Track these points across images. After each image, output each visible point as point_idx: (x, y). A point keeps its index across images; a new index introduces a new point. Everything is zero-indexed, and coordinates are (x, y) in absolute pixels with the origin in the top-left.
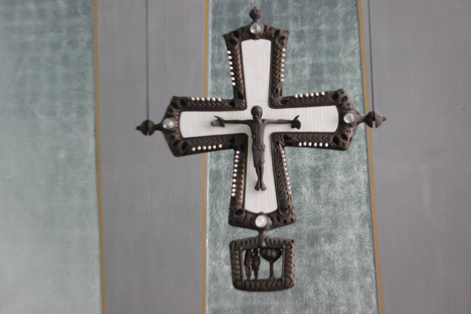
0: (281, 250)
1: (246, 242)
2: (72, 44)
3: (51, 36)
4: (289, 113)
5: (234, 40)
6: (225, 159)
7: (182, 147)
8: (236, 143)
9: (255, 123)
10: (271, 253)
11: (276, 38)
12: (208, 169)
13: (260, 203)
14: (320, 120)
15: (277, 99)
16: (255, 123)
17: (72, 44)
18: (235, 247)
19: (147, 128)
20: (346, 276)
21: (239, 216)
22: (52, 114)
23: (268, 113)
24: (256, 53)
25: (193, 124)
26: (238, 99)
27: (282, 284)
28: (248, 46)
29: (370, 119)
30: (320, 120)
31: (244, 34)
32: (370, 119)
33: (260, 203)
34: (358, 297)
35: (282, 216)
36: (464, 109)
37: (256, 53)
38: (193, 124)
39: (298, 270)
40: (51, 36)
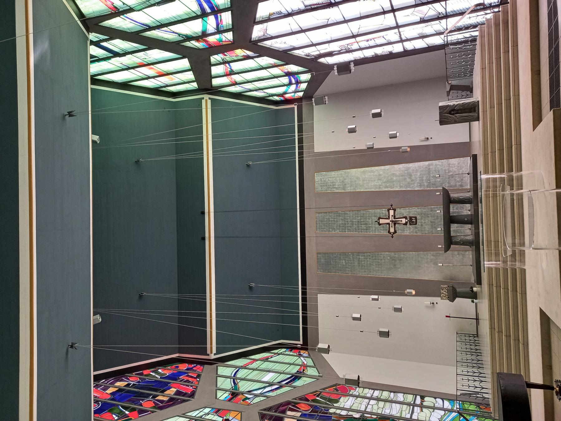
0: (411, 218)
2: (369, 256)
4: (391, 217)
6: (397, 225)
7: (395, 232)
9: (392, 221)
12: (481, 121)
13: (404, 221)
14: (392, 212)
15: (389, 218)
16: (392, 221)
17: (369, 256)
19: (392, 237)
20: (409, 212)
21: (406, 224)
22: (381, 260)
23: (391, 219)
24: (382, 221)
25: (392, 230)
26: (389, 224)
27: (416, 218)
29: (392, 206)
30: (392, 212)
32: (392, 206)
33: (404, 221)
34: (413, 210)
35: (406, 218)
37: (382, 221)
38: (392, 230)
39: (413, 216)
40: (368, 259)
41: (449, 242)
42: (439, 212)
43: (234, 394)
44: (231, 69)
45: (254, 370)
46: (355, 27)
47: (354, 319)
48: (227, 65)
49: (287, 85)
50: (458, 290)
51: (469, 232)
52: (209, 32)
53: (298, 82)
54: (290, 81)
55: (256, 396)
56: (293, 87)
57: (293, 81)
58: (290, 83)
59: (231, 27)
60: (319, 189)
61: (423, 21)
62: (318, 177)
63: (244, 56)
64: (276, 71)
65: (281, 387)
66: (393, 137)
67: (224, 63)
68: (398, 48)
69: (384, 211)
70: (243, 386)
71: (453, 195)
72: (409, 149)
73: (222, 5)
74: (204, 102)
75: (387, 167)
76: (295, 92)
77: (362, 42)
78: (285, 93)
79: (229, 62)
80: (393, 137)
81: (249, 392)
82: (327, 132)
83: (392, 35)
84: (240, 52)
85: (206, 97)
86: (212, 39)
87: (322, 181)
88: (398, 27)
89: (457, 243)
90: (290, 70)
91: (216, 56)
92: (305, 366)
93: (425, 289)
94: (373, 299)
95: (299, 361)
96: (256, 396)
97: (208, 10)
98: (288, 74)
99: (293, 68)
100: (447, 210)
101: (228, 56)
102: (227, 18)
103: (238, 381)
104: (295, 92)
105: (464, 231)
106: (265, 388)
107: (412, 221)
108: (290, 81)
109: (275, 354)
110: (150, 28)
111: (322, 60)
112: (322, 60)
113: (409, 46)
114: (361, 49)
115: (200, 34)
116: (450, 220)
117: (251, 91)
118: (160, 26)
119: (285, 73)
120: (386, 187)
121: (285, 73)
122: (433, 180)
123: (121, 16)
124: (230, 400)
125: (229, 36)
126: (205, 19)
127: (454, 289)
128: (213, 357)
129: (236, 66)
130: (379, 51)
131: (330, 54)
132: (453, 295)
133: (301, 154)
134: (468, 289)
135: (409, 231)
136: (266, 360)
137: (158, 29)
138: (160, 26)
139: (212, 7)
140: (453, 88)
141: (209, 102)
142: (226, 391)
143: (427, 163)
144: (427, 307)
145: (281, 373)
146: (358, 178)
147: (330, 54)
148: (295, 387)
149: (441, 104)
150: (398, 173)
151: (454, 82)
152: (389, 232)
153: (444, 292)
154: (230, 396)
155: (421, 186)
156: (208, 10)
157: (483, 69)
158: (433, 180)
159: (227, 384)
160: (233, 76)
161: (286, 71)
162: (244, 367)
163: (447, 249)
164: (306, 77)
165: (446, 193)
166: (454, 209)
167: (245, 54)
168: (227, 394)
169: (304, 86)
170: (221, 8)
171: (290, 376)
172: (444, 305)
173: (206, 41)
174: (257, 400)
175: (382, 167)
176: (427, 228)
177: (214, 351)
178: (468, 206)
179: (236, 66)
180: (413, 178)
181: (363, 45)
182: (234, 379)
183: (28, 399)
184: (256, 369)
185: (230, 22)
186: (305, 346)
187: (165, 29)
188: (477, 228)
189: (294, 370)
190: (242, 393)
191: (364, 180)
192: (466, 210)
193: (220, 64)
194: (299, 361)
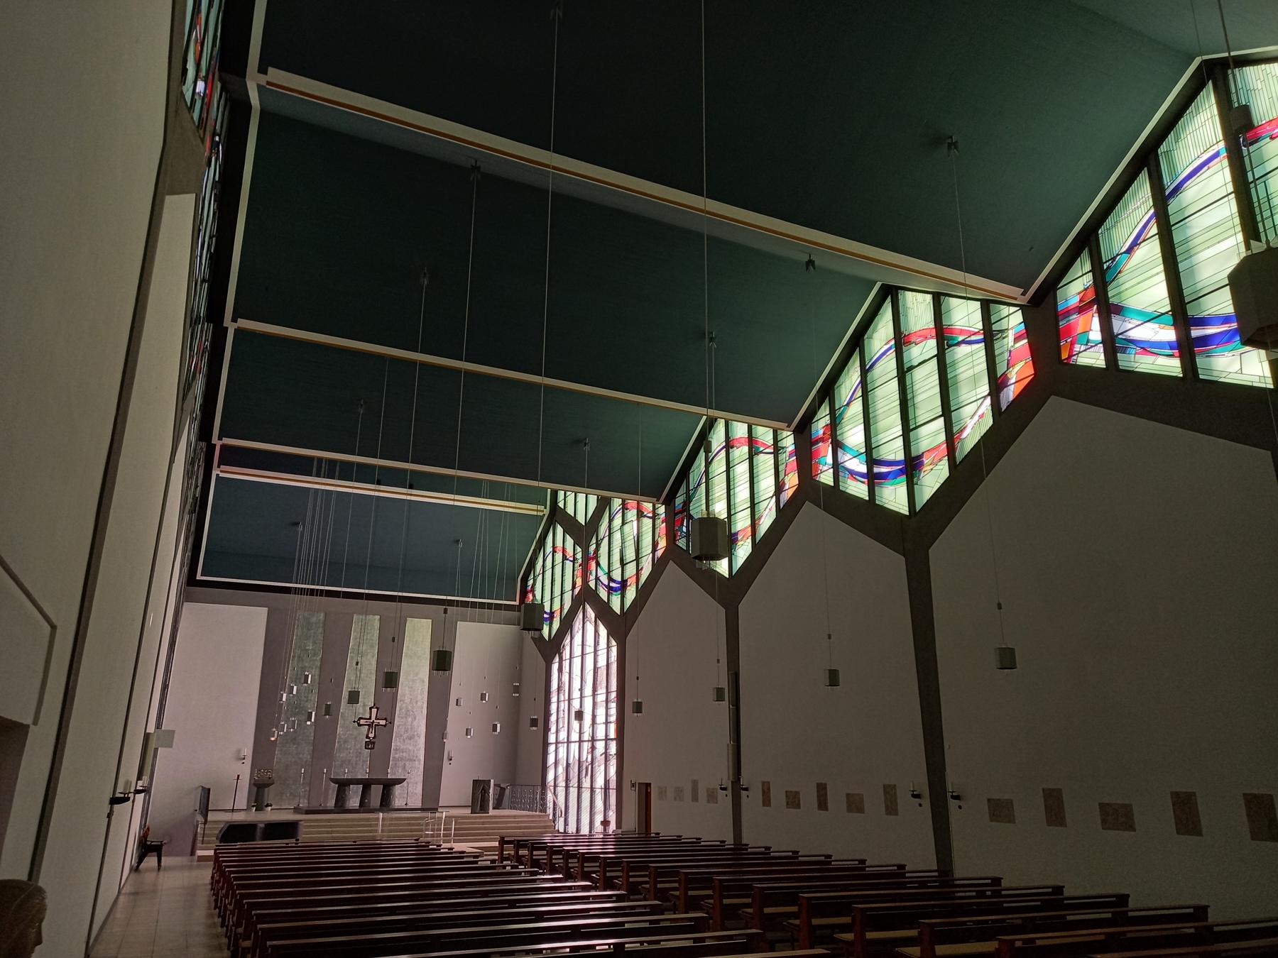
13: (371, 735)
25: (362, 722)
33: (371, 735)
38: (362, 722)
49: (609, 571)
52: (840, 452)
53: (610, 590)
54: (614, 581)
56: (604, 580)
58: (611, 579)
61: (568, 765)
63: (784, 484)
68: (552, 738)
74: (542, 508)
76: (597, 579)
78: (837, 445)
82: (479, 640)
83: (563, 735)
84: (792, 481)
85: (547, 512)
88: (569, 742)
97: (1196, 332)
98: (624, 584)
102: (858, 489)
104: (597, 579)
105: (354, 802)
108: (614, 581)
110: (865, 372)
111: (557, 659)
112: (557, 659)
113: (552, 748)
114: (558, 701)
118: (866, 389)
122: (401, 764)
125: (826, 478)
130: (553, 718)
131: (560, 670)
137: (1156, 214)
138: (866, 389)
140: (503, 790)
143: (422, 758)
144: (239, 751)
147: (560, 670)
150: (415, 723)
151: (507, 792)
157: (515, 817)
161: (926, 461)
164: (616, 607)
166: (376, 791)
169: (603, 594)
172: (245, 770)
173: (822, 440)
179: (765, 462)
181: (562, 704)
183: (45, 652)
186: (190, 580)
187: (859, 393)
192: (354, 802)
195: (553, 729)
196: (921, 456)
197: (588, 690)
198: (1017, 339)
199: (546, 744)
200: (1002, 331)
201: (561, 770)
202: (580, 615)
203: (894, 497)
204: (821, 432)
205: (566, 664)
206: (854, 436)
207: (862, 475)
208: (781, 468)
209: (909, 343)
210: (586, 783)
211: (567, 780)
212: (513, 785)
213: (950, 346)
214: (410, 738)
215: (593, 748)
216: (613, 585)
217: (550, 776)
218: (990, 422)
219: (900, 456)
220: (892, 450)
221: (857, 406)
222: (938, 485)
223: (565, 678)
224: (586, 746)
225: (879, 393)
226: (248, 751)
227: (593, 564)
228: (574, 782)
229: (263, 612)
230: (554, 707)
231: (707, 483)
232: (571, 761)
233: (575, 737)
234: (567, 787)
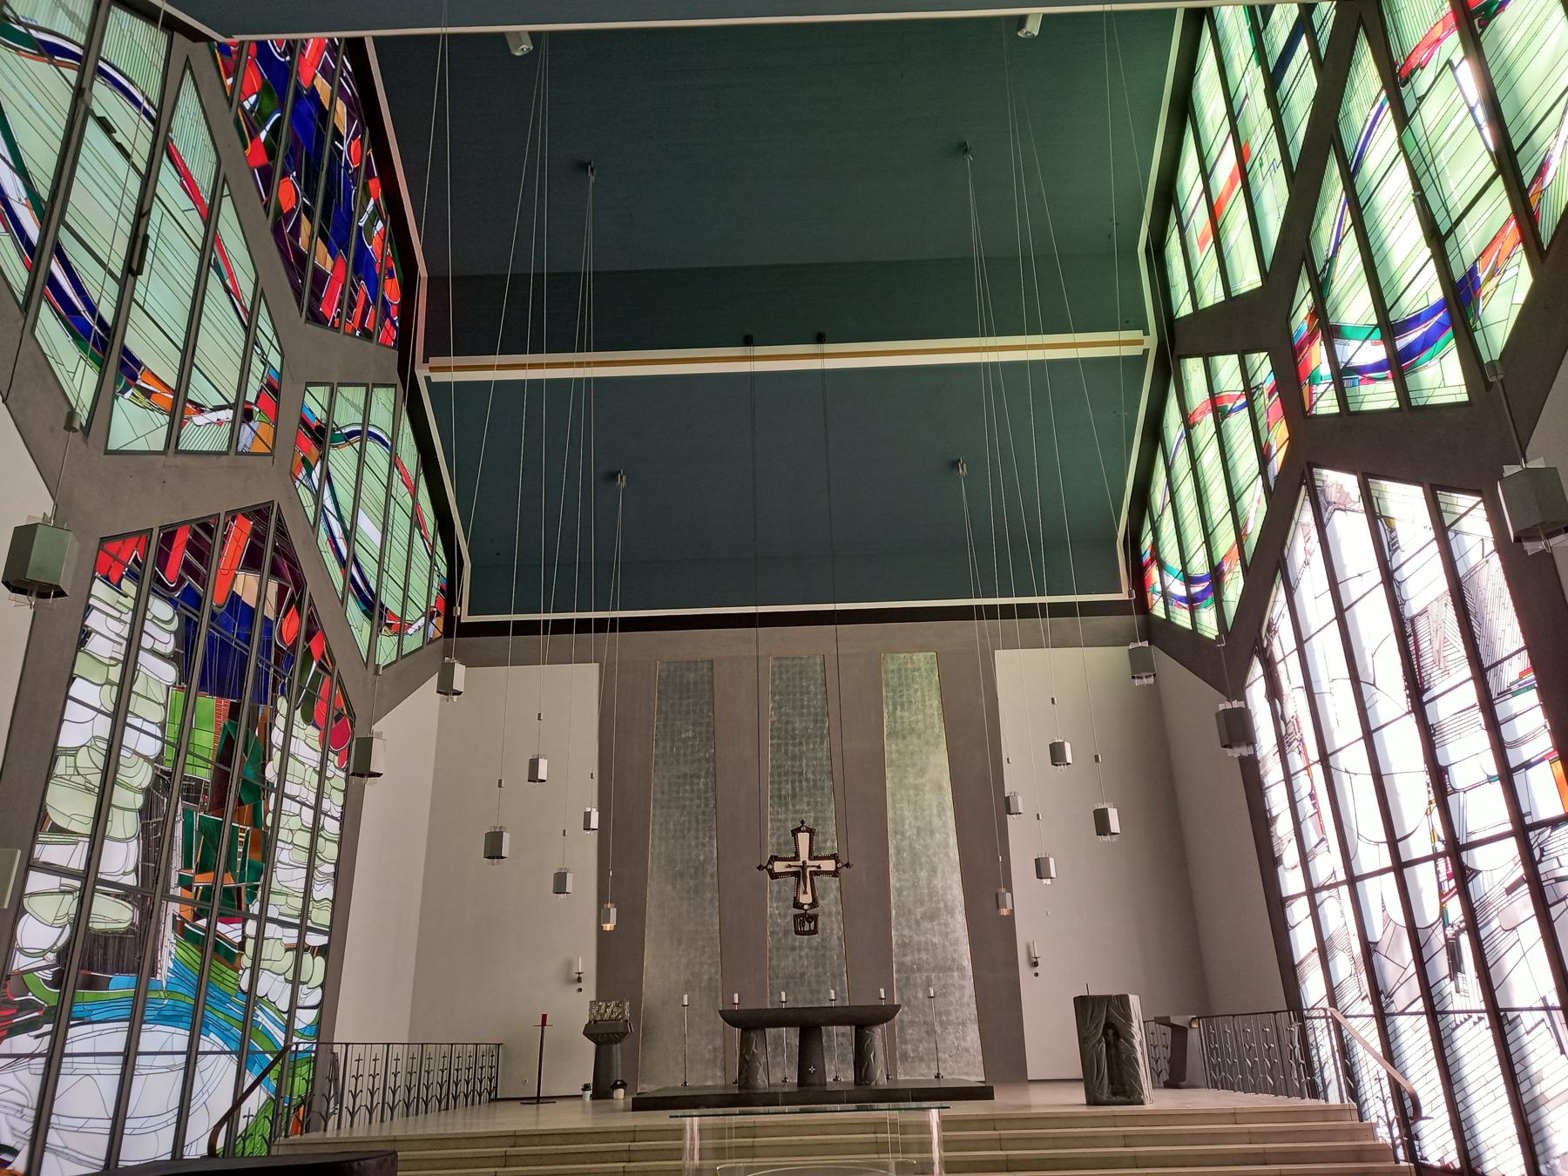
0: (814, 918)
1: (106, 939)
3: (697, 802)
4: (817, 863)
5: (795, 832)
6: (793, 879)
7: (774, 876)
8: (796, 874)
10: (129, 788)
11: (811, 832)
13: (806, 899)
14: (829, 865)
16: (804, 867)
18: (796, 917)
19: (760, 868)
21: (797, 905)
23: (809, 863)
24: (803, 838)
25: (779, 867)
26: (797, 857)
27: (815, 932)
28: (800, 835)
29: (847, 865)
30: (829, 865)
31: (799, 830)
32: (847, 865)
33: (806, 899)
35: (814, 904)
36: (1056, 753)
37: (803, 838)
38: (779, 867)
41: (750, 1024)
42: (832, 997)
43: (321, 435)
44: (1232, 411)
45: (388, 487)
46: (1352, 760)
47: (534, 764)
48: (1243, 400)
50: (617, 1048)
51: (777, 1077)
53: (1192, 602)
54: (1198, 580)
55: (317, 496)
56: (1178, 589)
57: (1196, 589)
59: (1353, 408)
60: (891, 664)
61: (1369, 949)
62: (923, 660)
63: (1269, 447)
64: (1225, 540)
65: (343, 564)
66: (1041, 869)
67: (1250, 391)
68: (1291, 881)
69: (831, 846)
70: (342, 460)
71: (878, 1034)
72: (1004, 912)
73: (1419, 383)
74: (1136, 334)
75: (954, 853)
76: (1165, 594)
77: (1311, 781)
78: (1331, 332)
79: (1250, 404)
80: (1041, 869)
81: (327, 477)
82: (1050, 688)
83: (1327, 864)
84: (1279, 436)
85: (1151, 342)
86: (1317, 356)
87: (914, 672)
88: (1352, 880)
89: (745, 1044)
90: (1228, 578)
91: (1267, 367)
92: (400, 630)
93: (618, 957)
94: (587, 816)
95: (413, 613)
96: (317, 496)
97: (1401, 343)
98: (1216, 575)
99: (1234, 587)
100: (838, 1016)
101: (1266, 403)
102: (1379, 396)
103: (357, 445)
106: (340, 519)
107: (805, 921)
108: (1198, 580)
109: (433, 547)
111: (1257, 669)
112: (1257, 669)
113: (1298, 912)
114: (1288, 778)
115: (1332, 321)
116: (810, 1025)
117: (1169, 469)
118: (1356, 206)
119: (1221, 564)
120: (898, 852)
121: (1221, 564)
122: (919, 978)
123: (1384, 94)
124: (304, 422)
125: (1326, 404)
126: (1377, 334)
127: (619, 1036)
128: (421, 373)
129: (1239, 424)
130: (1283, 828)
131: (1274, 692)
132: (603, 1035)
133: (990, 612)
134: (618, 1075)
135: (778, 913)
136: (416, 521)
138: (1356, 206)
139: (1412, 352)
140: (1179, 1033)
141: (1136, 351)
142: (330, 411)
143: (967, 963)
144: (569, 964)
145: (380, 563)
146: (922, 772)
147: (1274, 692)
148: (343, 602)
149: (1134, 1001)
150: (938, 882)
151: (1194, 1037)
152: (774, 859)
153: (610, 1010)
154: (315, 423)
155: (904, 945)
156: (1401, 343)
157: (1234, 1116)
158: (919, 978)
159: (347, 416)
160: (1210, 417)
161: (1226, 568)
162: (394, 462)
163: (731, 1018)
165: (885, 1014)
166: (839, 1038)
167: (1274, 450)
168: (319, 413)
169: (1182, 618)
170: (1409, 379)
171: (108, 316)
173: (1311, 338)
174: (307, 498)
175: (953, 840)
176: (787, 963)
177: (438, 377)
178: (848, 1076)
179: (1239, 424)
180: (926, 925)
181: (1302, 784)
182: (363, 434)
184: (389, 495)
185: (1366, 407)
186: (452, 627)
187: (1348, 221)
188: (789, 1099)
189: (391, 600)
190: (323, 457)
191: (916, 788)
192: (838, 1070)
193: (1246, 379)
194: (413, 613)
195: (1290, 855)
196: (1472, 273)
197: (1390, 697)
198: (1270, 395)
199: (1277, 904)
200: (1257, 387)
201: (1345, 965)
202: (1305, 515)
203: (1442, 379)
204: (1305, 327)
205: (1290, 674)
206: (1353, 305)
207: (1378, 367)
208: (1262, 423)
209: (1412, 73)
210: (1465, 994)
211: (1378, 994)
212: (1207, 1016)
213: (1484, 26)
214: (932, 916)
215: (1463, 876)
216: (1196, 589)
217: (1313, 990)
218: (1264, 507)
219: (1437, 294)
220: (1421, 290)
221: (1350, 253)
222: (1516, 311)
223: (1295, 703)
224: (1426, 880)
225: (1381, 199)
226: (586, 963)
227: (1154, 572)
228: (1406, 994)
229: (588, 674)
230: (1277, 799)
231: (1173, 501)
232: (1376, 932)
233: (1372, 856)
234: (1382, 1017)
